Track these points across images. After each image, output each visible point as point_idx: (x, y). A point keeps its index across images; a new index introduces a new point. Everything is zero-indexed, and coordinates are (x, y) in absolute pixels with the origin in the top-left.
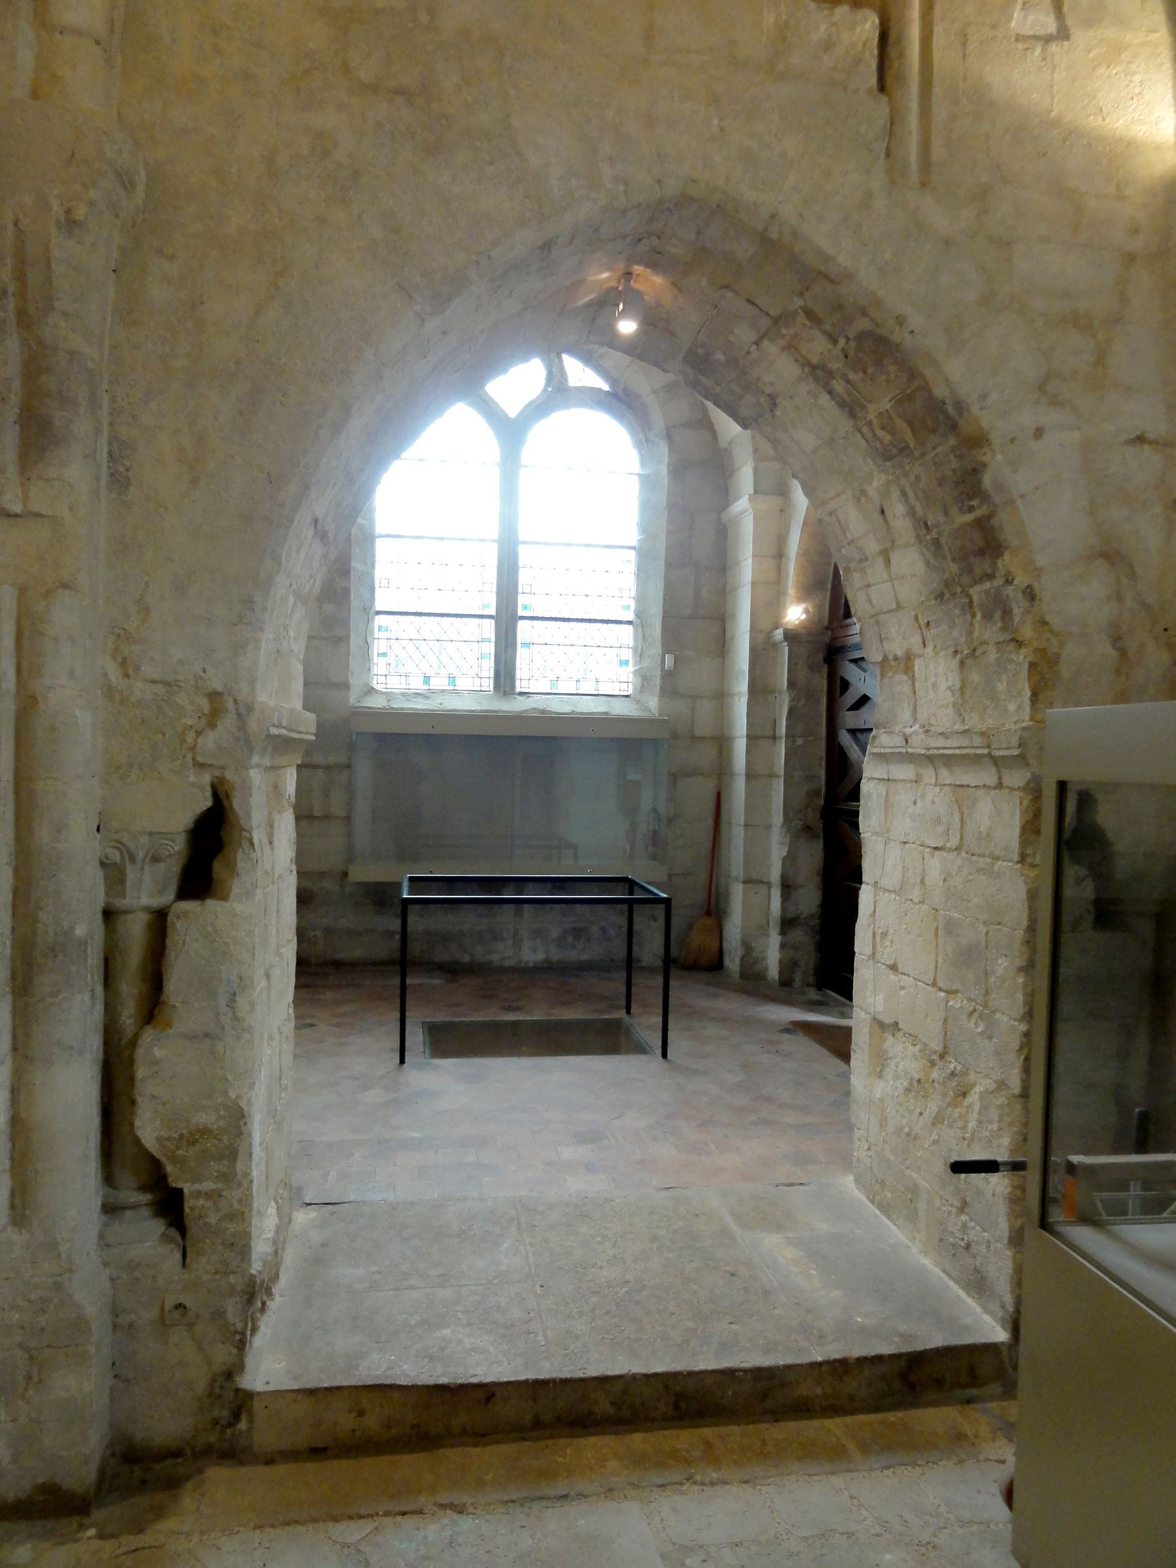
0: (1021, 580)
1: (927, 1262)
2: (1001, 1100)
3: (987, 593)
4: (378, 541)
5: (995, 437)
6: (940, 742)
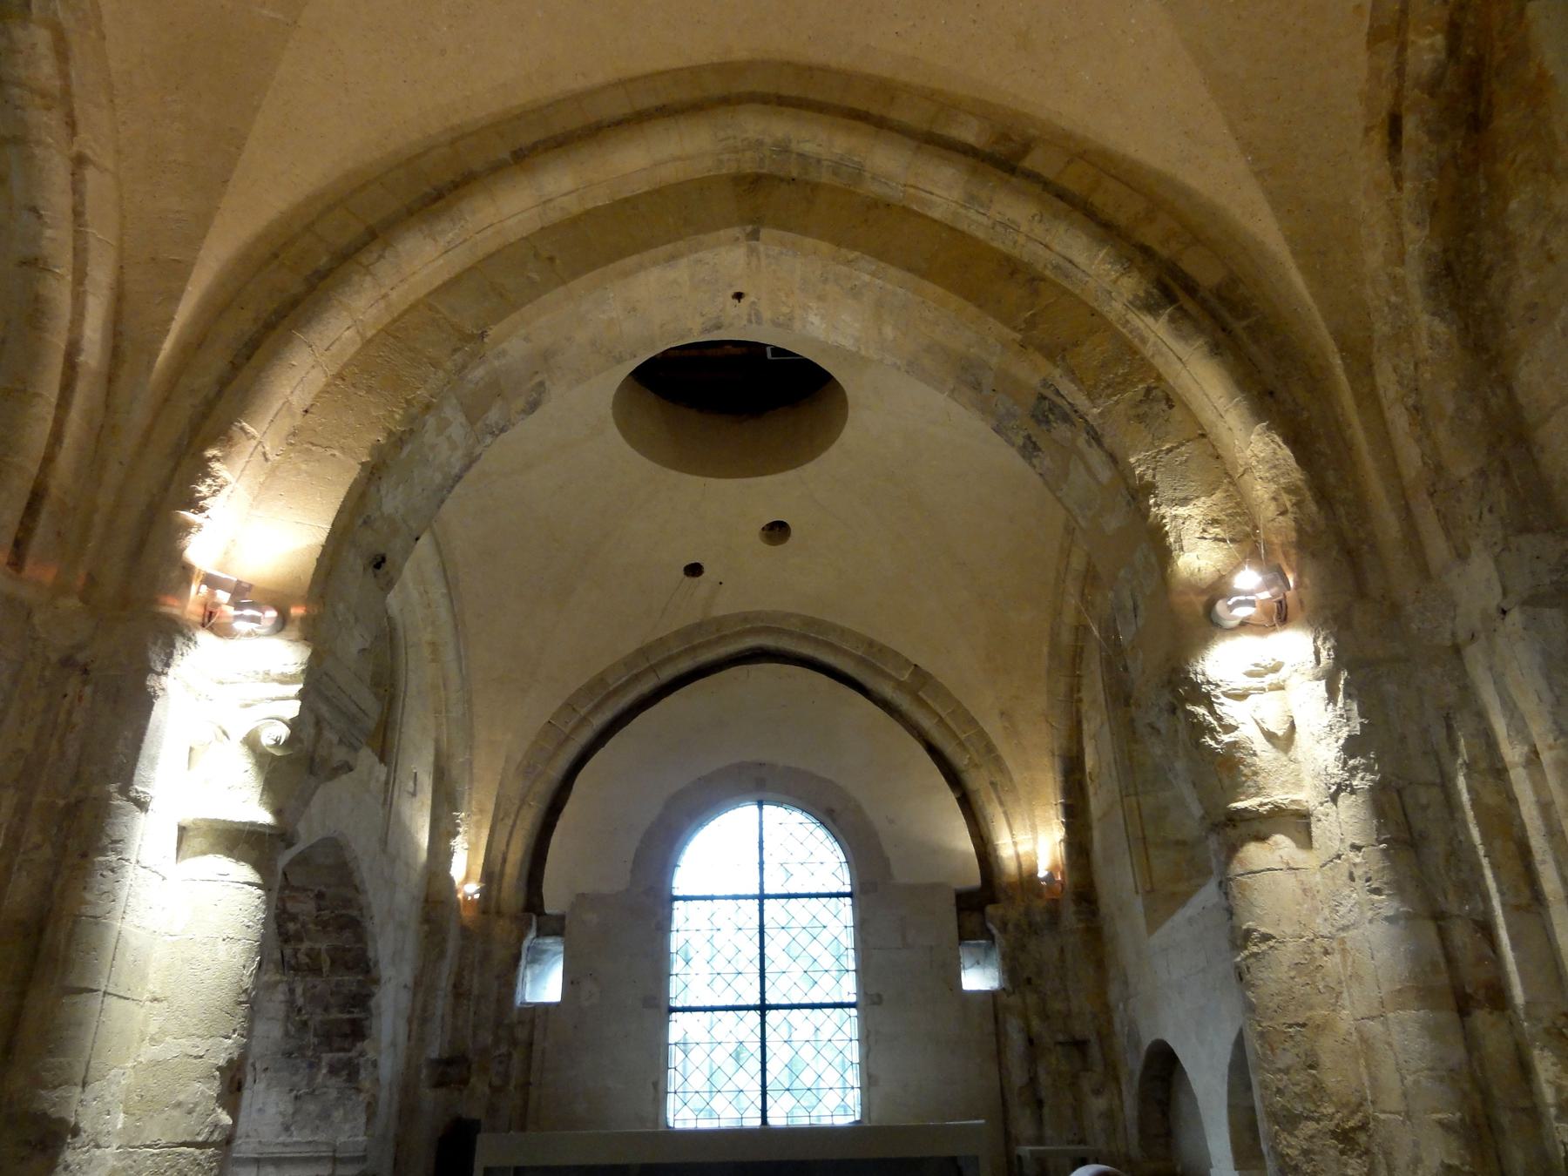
0: (371, 1055)
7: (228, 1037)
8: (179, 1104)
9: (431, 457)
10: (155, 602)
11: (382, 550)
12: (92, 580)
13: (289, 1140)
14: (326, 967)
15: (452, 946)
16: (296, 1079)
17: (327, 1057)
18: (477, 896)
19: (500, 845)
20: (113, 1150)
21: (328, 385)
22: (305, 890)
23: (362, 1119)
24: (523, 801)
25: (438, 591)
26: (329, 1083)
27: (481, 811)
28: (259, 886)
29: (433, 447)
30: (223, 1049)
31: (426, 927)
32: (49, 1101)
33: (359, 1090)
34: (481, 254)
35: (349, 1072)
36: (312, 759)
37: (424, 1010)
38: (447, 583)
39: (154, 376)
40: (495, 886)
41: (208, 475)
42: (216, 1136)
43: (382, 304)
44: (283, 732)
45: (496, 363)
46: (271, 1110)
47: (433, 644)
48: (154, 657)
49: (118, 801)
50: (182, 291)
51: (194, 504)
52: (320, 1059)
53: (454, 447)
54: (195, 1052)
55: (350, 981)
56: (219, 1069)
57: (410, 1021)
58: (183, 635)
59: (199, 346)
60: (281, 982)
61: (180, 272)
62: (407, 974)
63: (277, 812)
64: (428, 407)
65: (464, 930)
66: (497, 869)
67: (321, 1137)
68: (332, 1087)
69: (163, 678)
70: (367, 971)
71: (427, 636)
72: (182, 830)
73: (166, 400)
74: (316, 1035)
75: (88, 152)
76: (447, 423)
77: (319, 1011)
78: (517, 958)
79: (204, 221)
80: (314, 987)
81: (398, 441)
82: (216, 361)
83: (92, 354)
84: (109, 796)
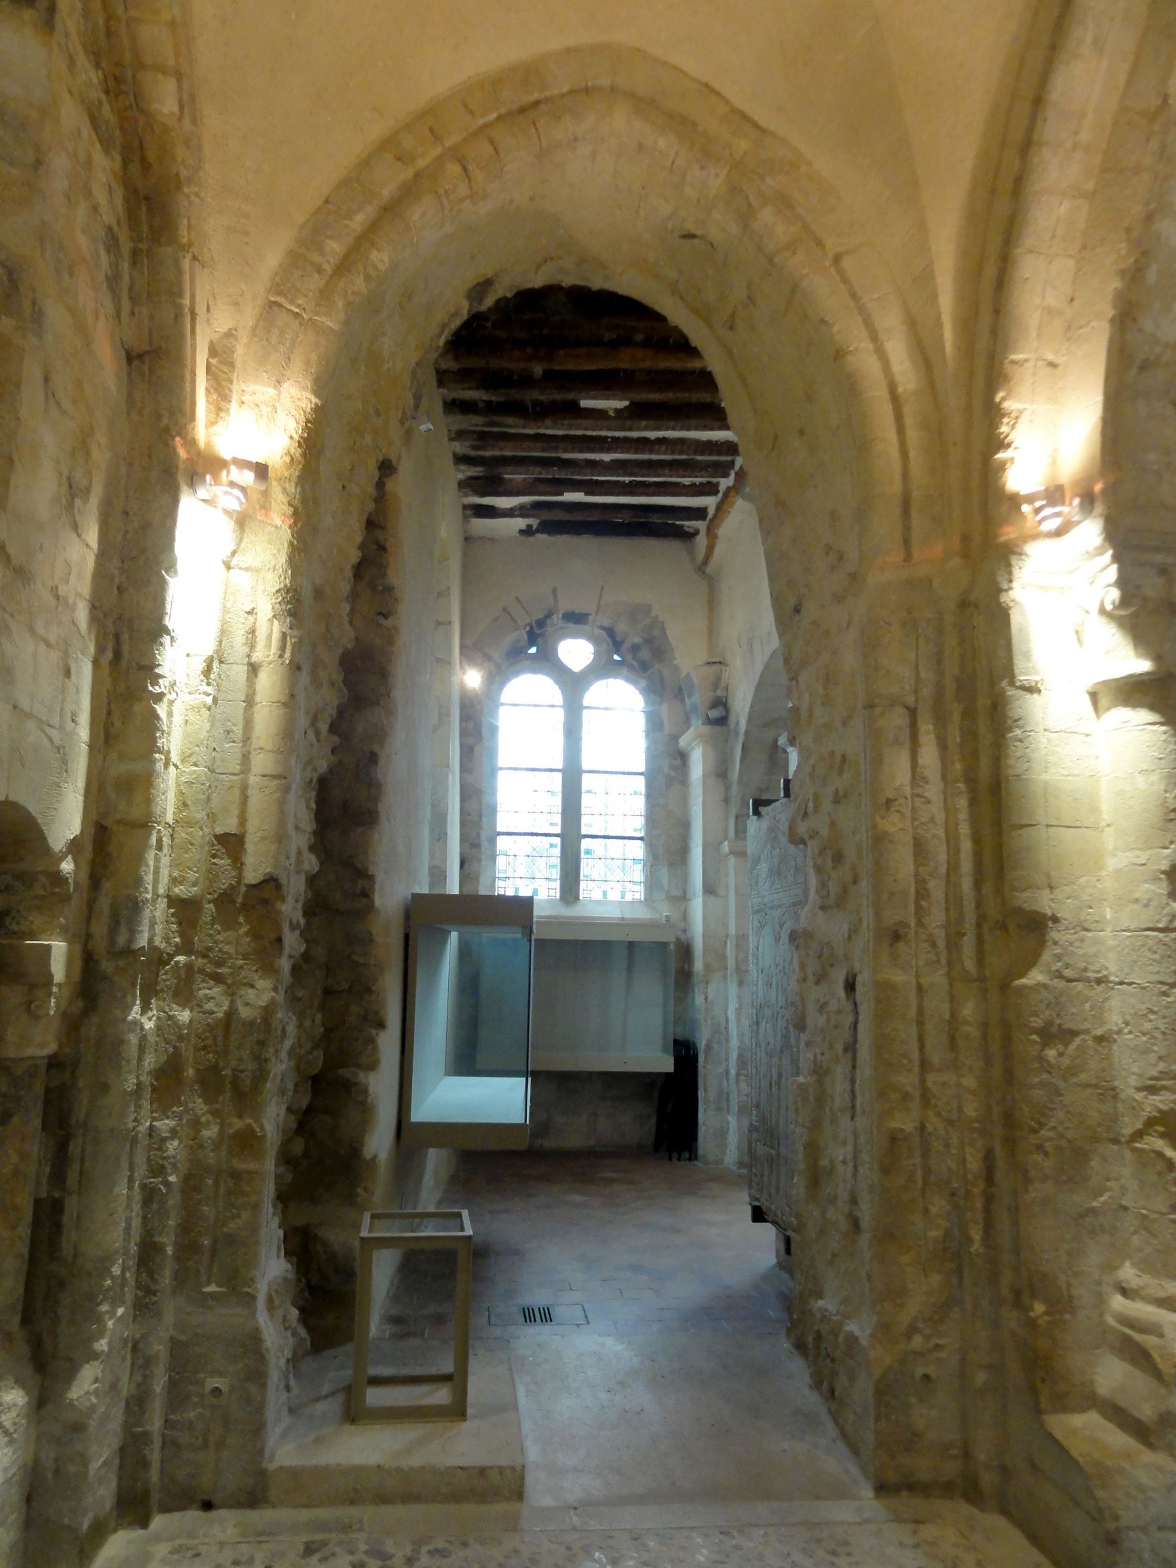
4: (642, 767)
7: (1167, 848)
8: (1137, 901)
28: (1162, 724)
32: (1023, 899)
41: (1003, 416)
44: (1115, 594)
48: (1000, 579)
49: (1011, 692)
51: (1003, 445)
56: (1163, 872)
61: (926, 278)
63: (1158, 658)
69: (1011, 592)
72: (1094, 696)
81: (1134, 275)
82: (986, 319)
84: (1003, 691)
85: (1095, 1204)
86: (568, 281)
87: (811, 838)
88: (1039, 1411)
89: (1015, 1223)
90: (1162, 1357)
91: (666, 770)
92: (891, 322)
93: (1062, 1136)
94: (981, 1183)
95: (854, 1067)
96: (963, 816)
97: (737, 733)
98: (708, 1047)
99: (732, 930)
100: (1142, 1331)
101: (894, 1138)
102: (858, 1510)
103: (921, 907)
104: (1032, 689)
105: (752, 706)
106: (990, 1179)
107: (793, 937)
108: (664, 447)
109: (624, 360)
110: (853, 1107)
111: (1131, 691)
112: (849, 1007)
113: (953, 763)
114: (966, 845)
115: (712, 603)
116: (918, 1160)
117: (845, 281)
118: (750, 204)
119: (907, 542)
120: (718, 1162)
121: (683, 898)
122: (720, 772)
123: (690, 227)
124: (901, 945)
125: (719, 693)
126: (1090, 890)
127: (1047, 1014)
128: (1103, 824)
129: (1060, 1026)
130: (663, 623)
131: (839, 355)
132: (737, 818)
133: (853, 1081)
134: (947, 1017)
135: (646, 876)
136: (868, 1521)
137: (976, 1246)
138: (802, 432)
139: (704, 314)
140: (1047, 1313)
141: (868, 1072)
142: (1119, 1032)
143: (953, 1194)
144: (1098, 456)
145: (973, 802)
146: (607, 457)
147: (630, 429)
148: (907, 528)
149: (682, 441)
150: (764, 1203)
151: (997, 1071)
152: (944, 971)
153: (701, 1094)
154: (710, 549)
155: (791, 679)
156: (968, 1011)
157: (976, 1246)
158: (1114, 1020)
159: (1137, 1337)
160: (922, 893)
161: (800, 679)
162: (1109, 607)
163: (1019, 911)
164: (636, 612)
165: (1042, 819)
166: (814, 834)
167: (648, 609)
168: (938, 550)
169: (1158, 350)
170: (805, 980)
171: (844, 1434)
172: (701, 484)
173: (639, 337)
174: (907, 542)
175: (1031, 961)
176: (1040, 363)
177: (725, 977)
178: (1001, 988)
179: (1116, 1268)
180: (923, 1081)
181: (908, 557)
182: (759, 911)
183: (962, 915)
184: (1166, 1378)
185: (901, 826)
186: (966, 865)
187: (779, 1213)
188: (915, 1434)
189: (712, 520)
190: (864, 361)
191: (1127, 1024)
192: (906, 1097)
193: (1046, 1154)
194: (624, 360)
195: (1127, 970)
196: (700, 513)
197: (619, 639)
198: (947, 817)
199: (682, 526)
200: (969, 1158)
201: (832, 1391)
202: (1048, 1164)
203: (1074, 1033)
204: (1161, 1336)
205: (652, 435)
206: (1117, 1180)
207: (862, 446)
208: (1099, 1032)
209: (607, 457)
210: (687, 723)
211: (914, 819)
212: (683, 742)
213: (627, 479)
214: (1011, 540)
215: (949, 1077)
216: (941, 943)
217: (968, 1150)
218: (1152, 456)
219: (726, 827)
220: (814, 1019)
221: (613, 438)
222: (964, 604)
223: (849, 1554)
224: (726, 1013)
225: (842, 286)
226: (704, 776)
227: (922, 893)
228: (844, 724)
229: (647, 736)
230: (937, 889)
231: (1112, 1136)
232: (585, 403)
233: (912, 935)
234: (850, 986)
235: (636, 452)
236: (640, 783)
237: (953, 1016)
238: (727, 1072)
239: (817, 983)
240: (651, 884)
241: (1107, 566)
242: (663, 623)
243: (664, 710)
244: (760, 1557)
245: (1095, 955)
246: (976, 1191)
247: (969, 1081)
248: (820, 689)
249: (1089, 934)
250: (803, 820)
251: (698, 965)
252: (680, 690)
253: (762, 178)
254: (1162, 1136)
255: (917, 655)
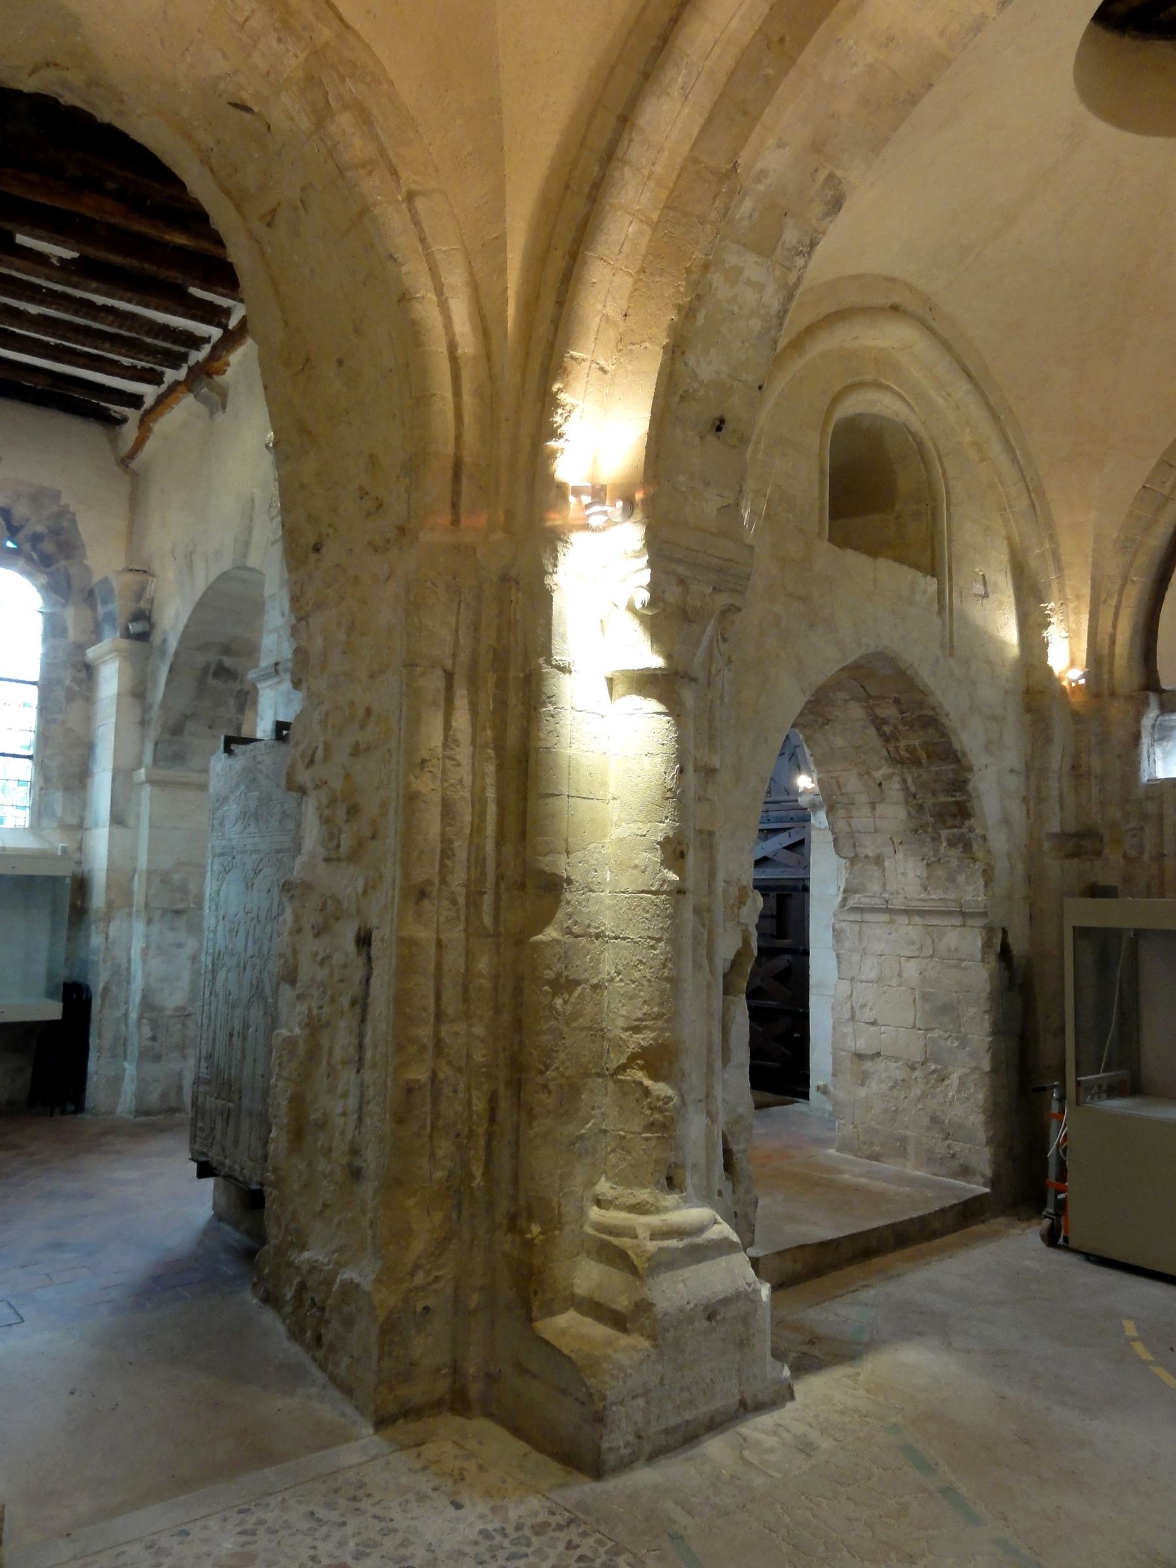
0: (979, 831)
1: (919, 1173)
2: (976, 1076)
3: (954, 835)
4: (36, 677)
5: (976, 769)
6: (918, 904)
8: (636, 867)
9: (736, 310)
10: (542, 520)
11: (716, 414)
12: (509, 514)
13: (927, 897)
14: (924, 761)
15: (1060, 730)
16: (925, 850)
17: (944, 833)
18: (1082, 681)
19: (1106, 624)
20: (607, 893)
21: (635, 283)
22: (884, 698)
23: (981, 883)
24: (1125, 579)
25: (961, 388)
26: (950, 853)
27: (1078, 597)
28: (666, 714)
29: (733, 300)
30: (662, 829)
31: (1029, 716)
33: (975, 860)
34: (722, 77)
35: (964, 844)
36: (684, 612)
37: (1038, 789)
38: (970, 376)
39: (509, 342)
40: (1105, 669)
41: (558, 406)
42: (665, 887)
43: (652, 184)
44: (646, 596)
45: (761, 187)
46: (911, 874)
47: (977, 444)
48: (545, 562)
49: (547, 669)
50: (505, 261)
51: (554, 434)
52: (940, 836)
53: (760, 287)
54: (639, 832)
55: (947, 768)
56: (658, 843)
57: (1025, 800)
58: (561, 540)
59: (538, 298)
60: (894, 773)
61: (498, 245)
62: (1013, 758)
63: (668, 657)
64: (706, 267)
65: (1076, 717)
66: (1106, 651)
67: (951, 895)
68: (953, 856)
70: (958, 761)
71: (968, 438)
72: (610, 681)
73: (527, 355)
74: (932, 816)
75: (413, 187)
76: (739, 270)
77: (929, 795)
78: (1137, 737)
79: (499, 194)
80: (920, 776)
81: (688, 313)
82: (548, 305)
83: (467, 345)
84: (540, 667)
85: (583, 1131)
86: (68, 99)
87: (317, 787)
88: (530, 1320)
89: (515, 1156)
90: (637, 1255)
91: (68, 682)
92: (455, 279)
93: (562, 1075)
94: (485, 1123)
95: (363, 1021)
96: (490, 780)
97: (163, 652)
98: (106, 989)
99: (143, 863)
100: (618, 1235)
101: (410, 1090)
102: (363, 1449)
103: (446, 866)
104: (564, 670)
105: (187, 627)
106: (492, 1118)
107: (286, 887)
108: (111, 318)
109: (87, 206)
110: (361, 1060)
111: (645, 683)
112: (361, 961)
113: (484, 729)
114: (492, 809)
115: (135, 502)
116: (428, 1107)
117: (416, 222)
118: (328, 102)
119: (455, 506)
120: (111, 1112)
121: (79, 827)
122: (137, 692)
123: (246, 97)
124: (426, 903)
125: (143, 604)
126: (596, 856)
127: (558, 967)
128: (610, 796)
129: (567, 977)
130: (74, 514)
131: (405, 298)
132: (156, 744)
133: (361, 1035)
134: (462, 971)
135: (34, 800)
136: (373, 1459)
137: (478, 1181)
138: (340, 362)
139: (238, 199)
140: (542, 1233)
141: (383, 1027)
142: (612, 980)
143: (458, 1135)
144: (641, 467)
145: (500, 768)
146: (34, 309)
147: (75, 286)
148: (456, 494)
149: (134, 317)
150: (214, 1156)
151: (506, 1017)
152: (462, 927)
153: (93, 1041)
154: (140, 443)
155: (300, 619)
156: (483, 964)
157: (478, 1181)
158: (607, 969)
159: (615, 1241)
160: (447, 852)
161: (311, 620)
162: (638, 606)
163: (541, 873)
164: (38, 496)
165: (565, 791)
166: (321, 784)
167: (57, 495)
168: (482, 520)
169: (696, 385)
170: (299, 931)
171: (333, 1378)
172: (143, 368)
173: (111, 186)
174: (455, 506)
175: (546, 920)
176: (594, 365)
177: (130, 915)
178: (517, 943)
179: (595, 1184)
180: (437, 1033)
181: (456, 521)
182: (222, 854)
183: (483, 873)
184: (641, 1272)
185: (432, 786)
186: (490, 828)
187: (237, 1167)
188: (412, 1364)
189: (148, 412)
190: (428, 311)
191: (619, 973)
192: (423, 1048)
193: (550, 1092)
194: (87, 206)
195: (622, 927)
196: (135, 401)
197: (15, 524)
198: (473, 782)
199: (107, 409)
200: (474, 1100)
201: (318, 1339)
202: (550, 1101)
203: (577, 983)
204: (636, 1237)
205: (100, 300)
206: (600, 1108)
207: (421, 399)
208: (595, 981)
209: (34, 309)
210: (97, 637)
211: (443, 780)
212: (91, 653)
213: (53, 341)
214: (556, 526)
215: (461, 1027)
216: (461, 901)
217: (474, 1093)
218: (681, 478)
219: (142, 752)
220: (307, 971)
221: (50, 290)
222: (505, 578)
223: (369, 1495)
224: (129, 954)
225: (413, 226)
226: (119, 694)
227: (447, 852)
228: (372, 676)
229: (45, 639)
230: (461, 848)
231: (599, 1070)
232: (21, 239)
233: (435, 893)
234: (364, 940)
235: (76, 313)
236: (32, 695)
237: (467, 969)
238: (126, 1015)
239: (317, 935)
240: (40, 810)
241: (642, 569)
242: (74, 514)
243: (69, 615)
244: (287, 1525)
245: (597, 913)
246: (481, 1131)
247: (479, 1030)
248: (342, 636)
249: (594, 895)
250: (307, 768)
251: (98, 899)
252: (91, 593)
253: (342, 79)
254: (641, 1068)
255: (457, 622)
